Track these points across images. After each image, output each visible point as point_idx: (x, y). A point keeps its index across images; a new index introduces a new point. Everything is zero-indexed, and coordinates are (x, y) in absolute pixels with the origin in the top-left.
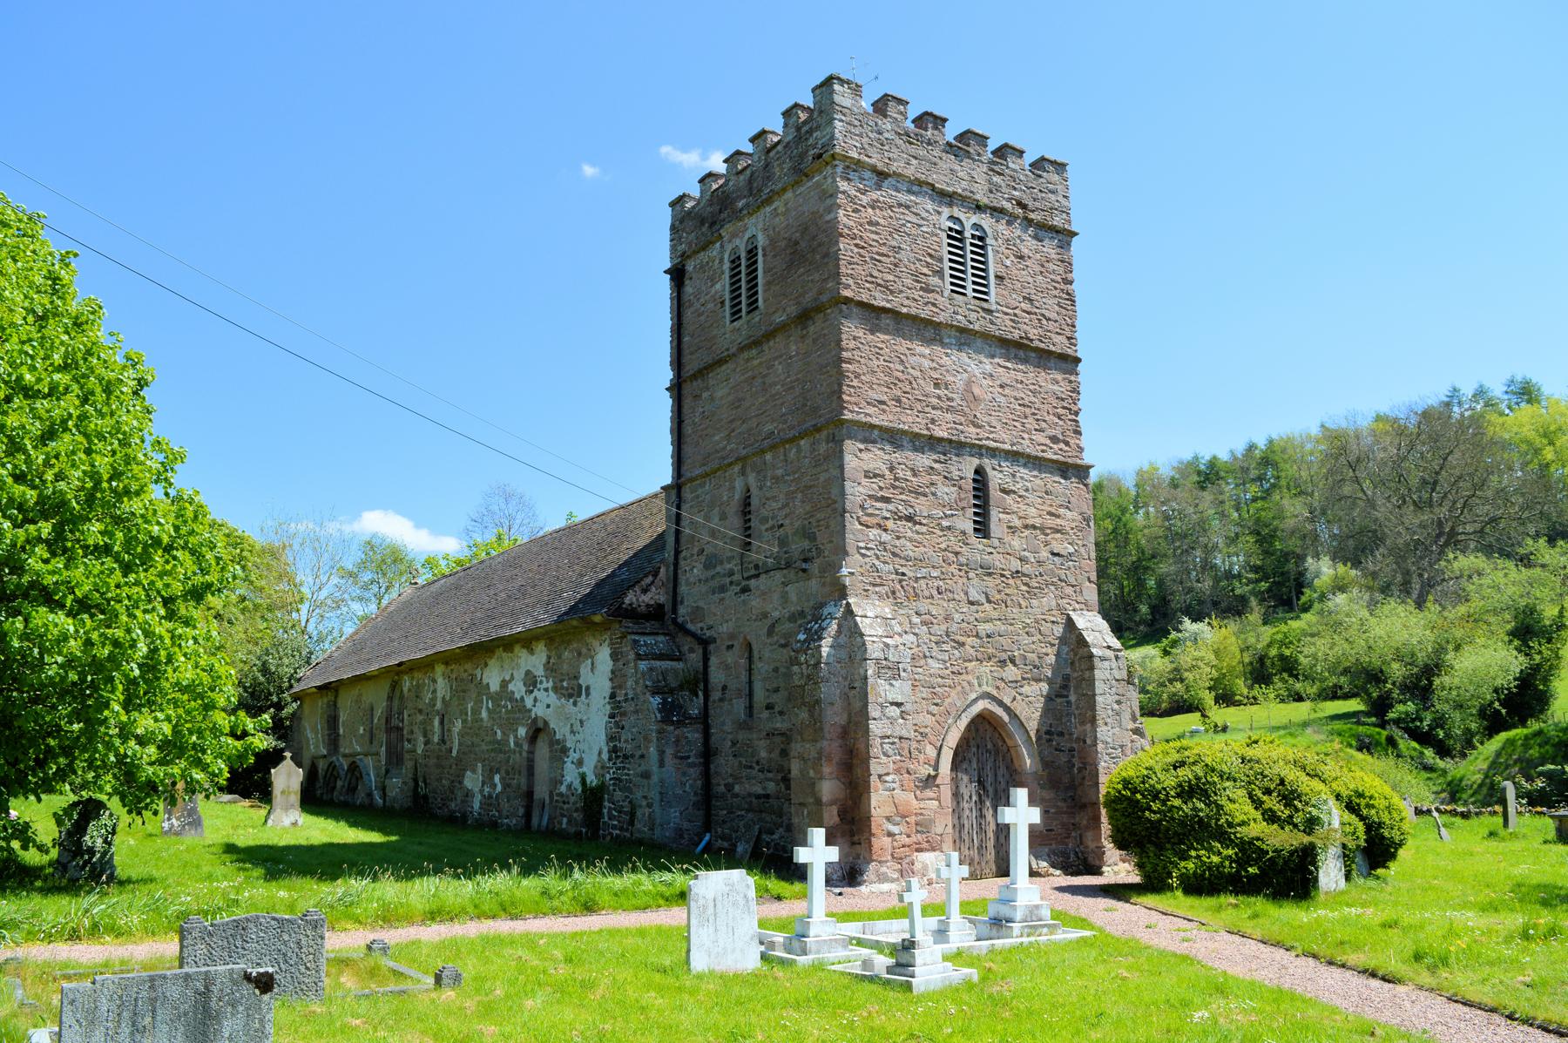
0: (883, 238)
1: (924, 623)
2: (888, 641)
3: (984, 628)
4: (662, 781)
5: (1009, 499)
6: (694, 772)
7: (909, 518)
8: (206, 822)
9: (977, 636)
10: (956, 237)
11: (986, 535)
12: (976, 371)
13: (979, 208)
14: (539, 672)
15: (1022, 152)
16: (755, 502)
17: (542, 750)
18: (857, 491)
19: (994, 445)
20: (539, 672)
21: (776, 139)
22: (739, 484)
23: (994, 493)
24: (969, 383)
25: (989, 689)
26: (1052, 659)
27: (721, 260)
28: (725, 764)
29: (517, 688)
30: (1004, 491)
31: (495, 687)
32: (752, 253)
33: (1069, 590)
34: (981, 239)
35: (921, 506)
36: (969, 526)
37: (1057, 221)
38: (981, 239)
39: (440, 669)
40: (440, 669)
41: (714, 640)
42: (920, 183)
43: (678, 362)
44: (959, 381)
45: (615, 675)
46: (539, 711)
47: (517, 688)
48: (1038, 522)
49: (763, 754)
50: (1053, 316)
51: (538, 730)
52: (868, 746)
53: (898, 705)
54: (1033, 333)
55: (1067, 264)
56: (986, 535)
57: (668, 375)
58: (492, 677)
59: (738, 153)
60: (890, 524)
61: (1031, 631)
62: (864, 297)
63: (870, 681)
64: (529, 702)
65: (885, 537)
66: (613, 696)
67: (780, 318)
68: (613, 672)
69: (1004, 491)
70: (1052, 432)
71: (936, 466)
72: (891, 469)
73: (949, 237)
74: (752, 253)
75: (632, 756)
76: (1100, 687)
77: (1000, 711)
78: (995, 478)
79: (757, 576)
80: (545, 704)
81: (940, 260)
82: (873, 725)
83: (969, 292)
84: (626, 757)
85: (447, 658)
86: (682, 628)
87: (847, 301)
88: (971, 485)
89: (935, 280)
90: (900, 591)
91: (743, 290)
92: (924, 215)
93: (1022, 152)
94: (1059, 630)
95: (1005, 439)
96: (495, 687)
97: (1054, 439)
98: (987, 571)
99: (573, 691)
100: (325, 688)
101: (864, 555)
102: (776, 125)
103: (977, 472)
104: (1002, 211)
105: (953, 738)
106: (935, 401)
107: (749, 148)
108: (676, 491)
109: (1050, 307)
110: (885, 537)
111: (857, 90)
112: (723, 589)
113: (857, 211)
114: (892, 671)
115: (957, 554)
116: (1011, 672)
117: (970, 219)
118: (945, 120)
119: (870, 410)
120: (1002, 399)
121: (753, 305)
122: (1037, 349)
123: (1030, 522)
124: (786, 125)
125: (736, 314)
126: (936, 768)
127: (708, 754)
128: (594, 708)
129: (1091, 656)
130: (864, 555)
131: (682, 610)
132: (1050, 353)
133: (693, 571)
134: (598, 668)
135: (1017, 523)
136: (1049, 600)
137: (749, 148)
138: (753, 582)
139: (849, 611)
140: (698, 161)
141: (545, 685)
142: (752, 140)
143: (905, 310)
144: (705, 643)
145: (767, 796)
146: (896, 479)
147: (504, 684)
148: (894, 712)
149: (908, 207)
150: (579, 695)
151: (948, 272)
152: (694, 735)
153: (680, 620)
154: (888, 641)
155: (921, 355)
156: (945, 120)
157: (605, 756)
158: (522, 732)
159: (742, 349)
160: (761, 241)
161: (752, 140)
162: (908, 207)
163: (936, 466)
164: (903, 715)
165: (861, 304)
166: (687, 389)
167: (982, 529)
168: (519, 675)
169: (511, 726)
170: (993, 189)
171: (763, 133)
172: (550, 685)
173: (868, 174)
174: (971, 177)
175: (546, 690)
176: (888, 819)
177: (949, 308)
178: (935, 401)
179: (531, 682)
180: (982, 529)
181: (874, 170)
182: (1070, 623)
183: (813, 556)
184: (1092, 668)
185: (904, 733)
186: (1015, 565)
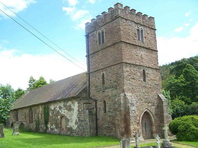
0: (128, 30)
1: (137, 97)
2: (132, 100)
3: (146, 97)
4: (90, 125)
5: (148, 75)
6: (95, 123)
7: (134, 79)
8: (5, 135)
9: (145, 98)
10: (138, 30)
11: (145, 81)
12: (143, 53)
13: (141, 25)
14: (62, 106)
15: (147, 16)
16: (105, 76)
17: (63, 120)
18: (126, 74)
19: (146, 66)
20: (62, 106)
21: (107, 13)
22: (102, 73)
23: (146, 74)
24: (141, 55)
25: (147, 107)
26: (156, 102)
27: (97, 34)
28: (100, 122)
29: (58, 109)
30: (147, 74)
31: (53, 109)
32: (103, 33)
33: (158, 90)
34: (142, 31)
35: (135, 77)
36: (143, 80)
37: (153, 28)
38: (142, 31)
39: (40, 106)
40: (40, 106)
41: (97, 100)
42: (132, 21)
43: (88, 51)
44: (140, 55)
45: (79, 107)
46: (63, 113)
47: (58, 109)
48: (153, 79)
49: (108, 120)
50: (153, 44)
51: (62, 117)
52: (130, 118)
53: (134, 110)
54: (151, 47)
55: (155, 35)
56: (145, 81)
57: (86, 54)
58: (52, 107)
59: (99, 15)
60: (131, 80)
61: (152, 96)
62: (125, 41)
63: (130, 107)
64: (60, 111)
65: (130, 82)
66: (79, 110)
67: (109, 44)
68: (78, 106)
69: (147, 74)
70: (154, 64)
71: (137, 70)
72: (130, 70)
73: (137, 30)
74: (103, 33)
75: (83, 121)
76: (164, 106)
77: (148, 111)
78: (146, 72)
79: (106, 89)
80: (64, 112)
81: (136, 34)
82: (130, 114)
83: (141, 40)
84: (82, 121)
85: (42, 104)
86: (91, 98)
87: (122, 42)
88: (142, 73)
89: (135, 38)
90: (133, 91)
91: (101, 39)
92: (133, 26)
93: (147, 16)
94: (157, 97)
95: (147, 65)
96: (53, 109)
97: (154, 65)
98: (145, 87)
99: (70, 109)
100: (15, 110)
101: (127, 85)
102: (107, 11)
103: (143, 71)
104: (145, 26)
105: (142, 115)
106: (136, 59)
107: (101, 15)
108: (89, 74)
109: (153, 42)
110: (130, 82)
111: (122, 5)
112: (99, 91)
113: (123, 25)
114: (132, 104)
115: (141, 84)
116: (150, 104)
117: (140, 28)
118: (136, 10)
119: (127, 60)
120: (146, 58)
121: (103, 42)
122: (151, 49)
123: (152, 79)
124: (109, 11)
125: (100, 43)
126: (139, 121)
127: (97, 120)
128: (75, 112)
129: (162, 101)
130: (127, 85)
131: (90, 95)
132: (153, 50)
133: (92, 89)
134: (75, 106)
135: (150, 79)
136: (155, 92)
137: (101, 15)
138: (105, 90)
139: (125, 95)
140: (146, 14)
141: (64, 108)
142: (102, 13)
143: (131, 43)
144: (96, 101)
145: (109, 127)
146: (131, 72)
147: (55, 108)
148: (133, 112)
149: (130, 25)
150: (71, 110)
151: (137, 36)
152: (94, 117)
153: (90, 97)
154: (132, 100)
155: (134, 51)
156: (136, 10)
157: (77, 121)
158: (59, 117)
159: (101, 50)
160: (104, 31)
161: (102, 13)
162: (130, 25)
163: (137, 70)
164: (135, 112)
165: (125, 42)
166: (90, 56)
167: (144, 80)
168: (58, 107)
169: (57, 116)
170: (143, 22)
171: (104, 12)
172: (65, 108)
173: (124, 20)
174: (140, 20)
175: (64, 109)
176: (133, 130)
177: (138, 43)
178: (136, 59)
179: (60, 108)
180: (144, 80)
181: (125, 19)
182: (158, 96)
183: (118, 85)
184: (163, 103)
185: (135, 115)
186: (150, 86)
